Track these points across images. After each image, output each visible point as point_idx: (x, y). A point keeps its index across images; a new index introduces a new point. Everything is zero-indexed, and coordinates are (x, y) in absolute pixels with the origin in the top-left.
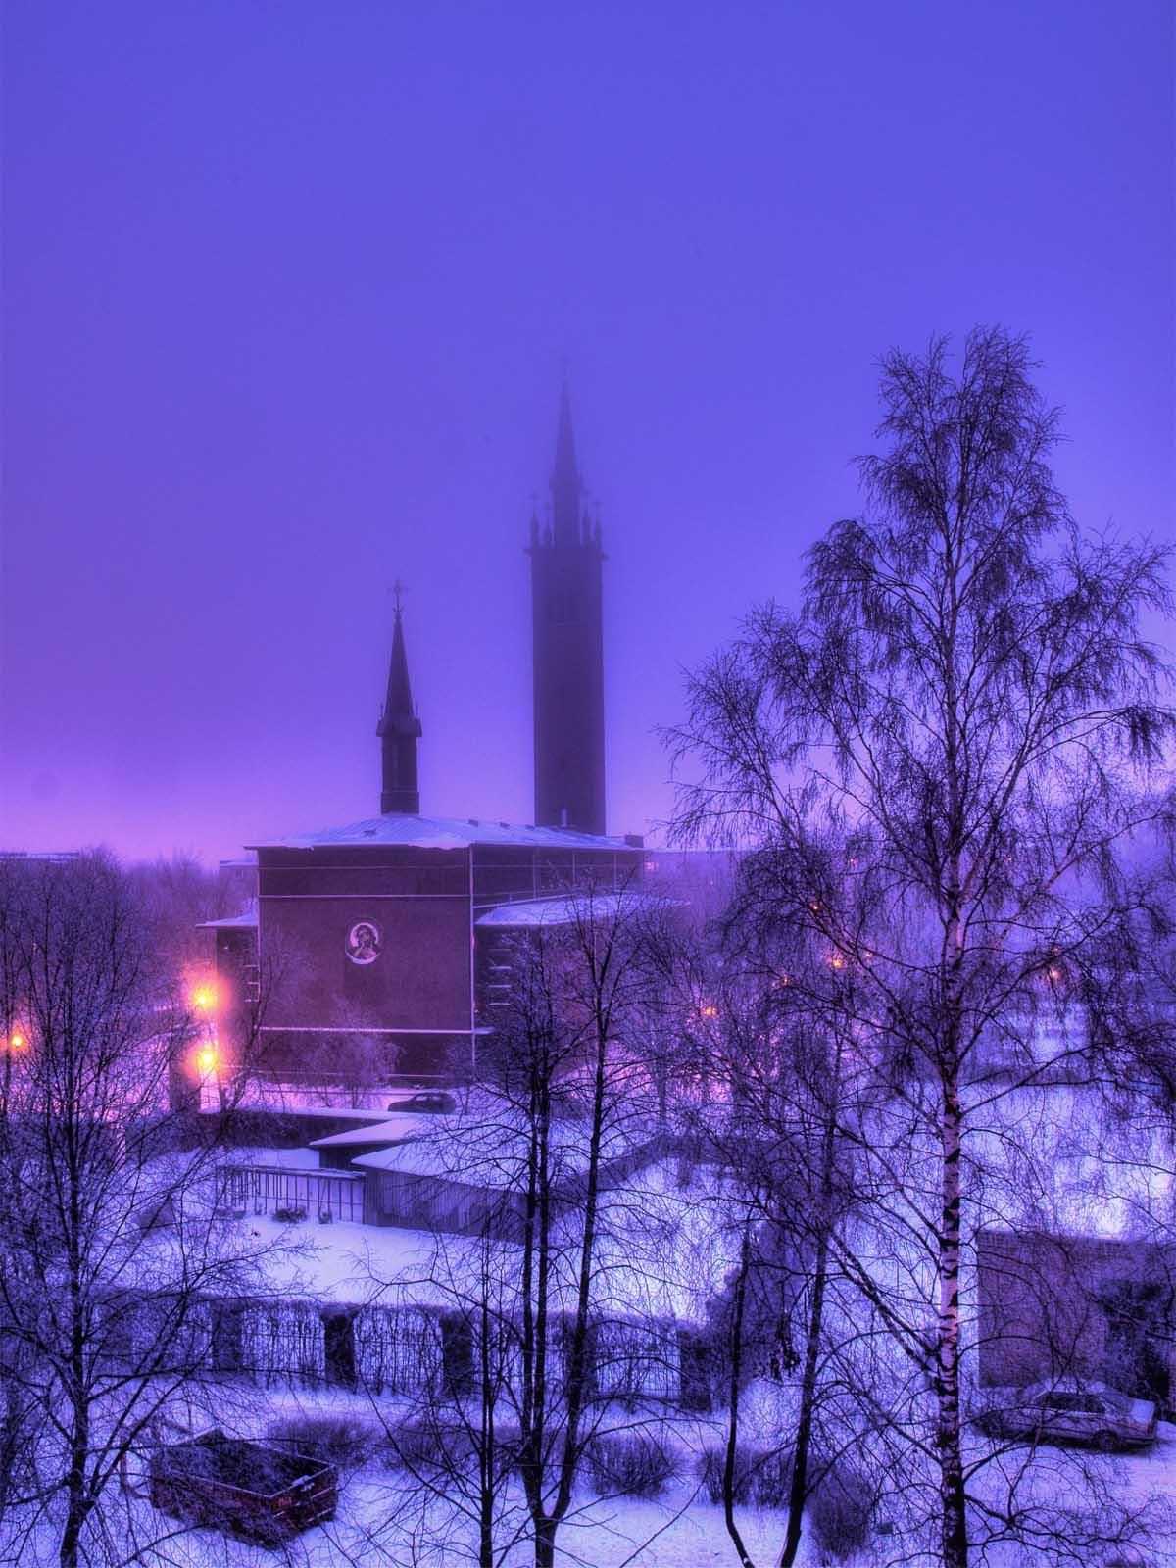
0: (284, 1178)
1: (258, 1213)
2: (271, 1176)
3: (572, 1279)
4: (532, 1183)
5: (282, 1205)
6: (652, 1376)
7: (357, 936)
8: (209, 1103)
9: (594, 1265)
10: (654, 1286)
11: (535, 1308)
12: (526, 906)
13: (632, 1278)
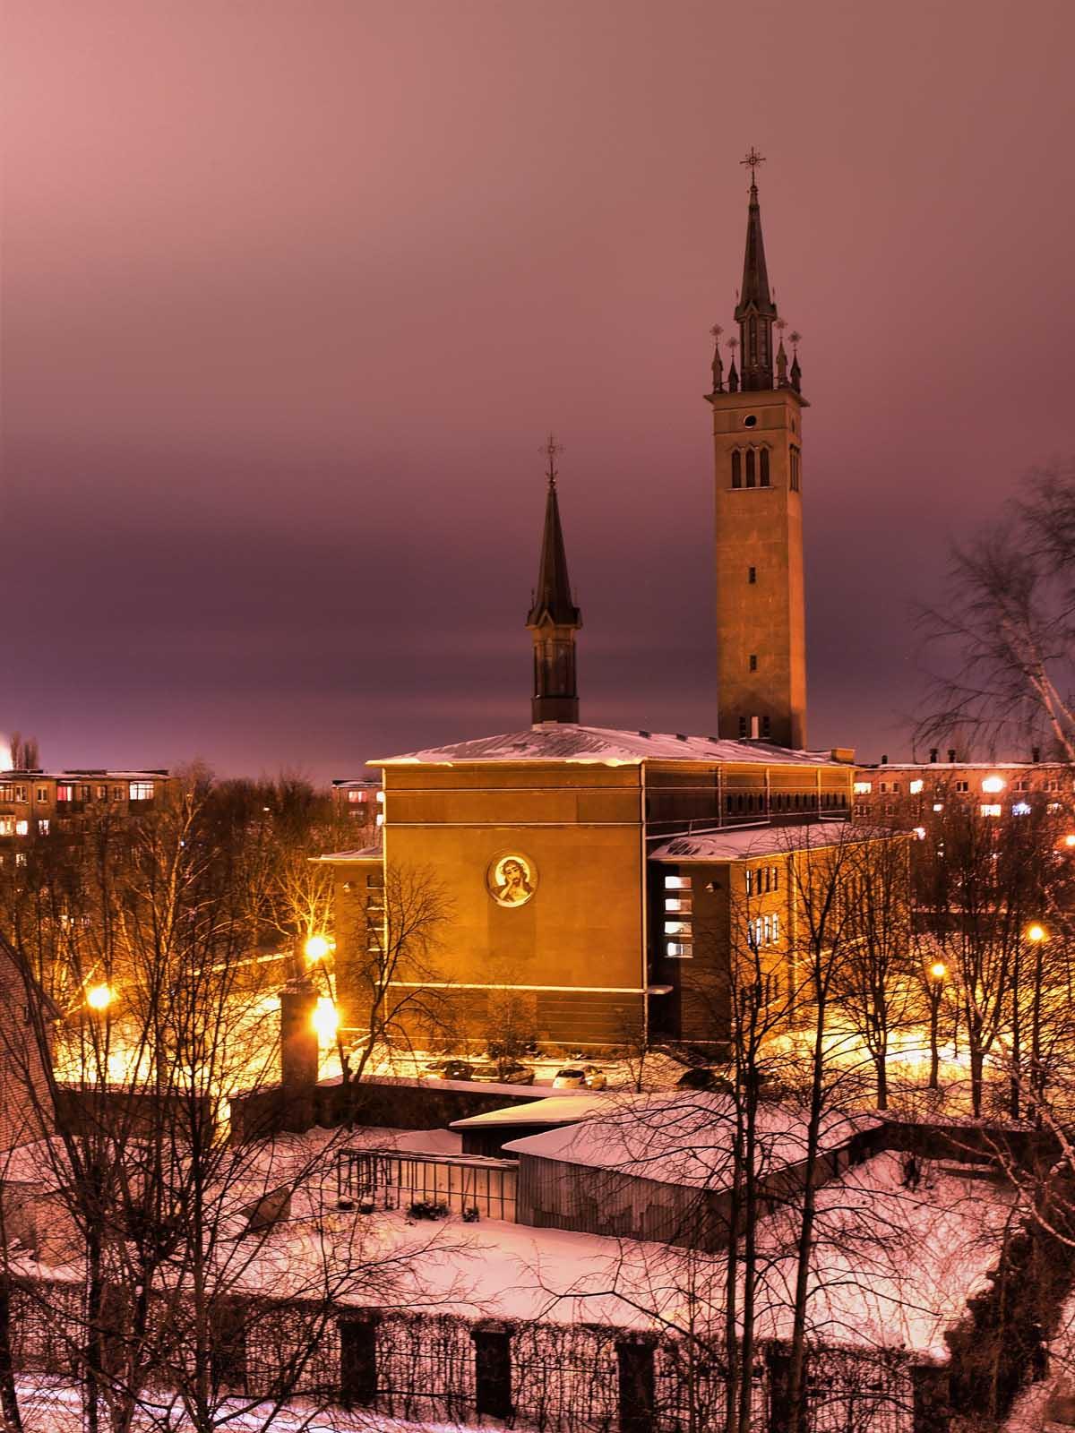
0: (420, 1165)
1: (389, 1208)
2: (404, 1164)
3: (784, 1294)
4: (736, 1177)
5: (419, 1198)
6: (877, 1421)
7: (505, 872)
8: (329, 1071)
9: (812, 1281)
10: (887, 1307)
11: (739, 1331)
12: (710, 837)
13: (860, 1298)
